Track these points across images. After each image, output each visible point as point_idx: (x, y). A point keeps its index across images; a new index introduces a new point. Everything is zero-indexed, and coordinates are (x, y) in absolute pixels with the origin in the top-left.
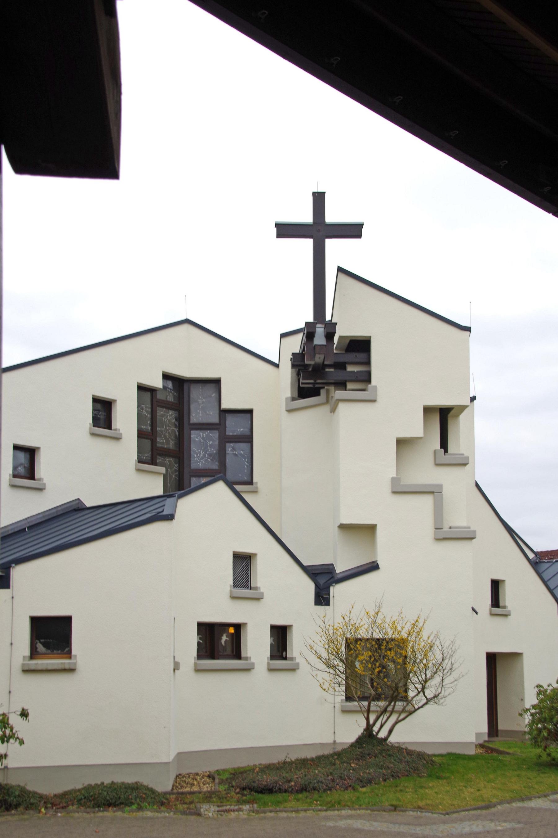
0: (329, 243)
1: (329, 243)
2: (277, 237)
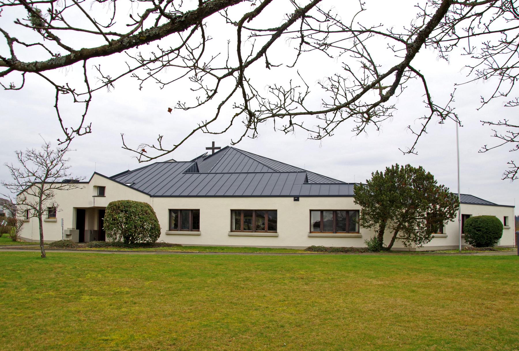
0: (211, 147)
1: (211, 147)
2: (199, 210)
